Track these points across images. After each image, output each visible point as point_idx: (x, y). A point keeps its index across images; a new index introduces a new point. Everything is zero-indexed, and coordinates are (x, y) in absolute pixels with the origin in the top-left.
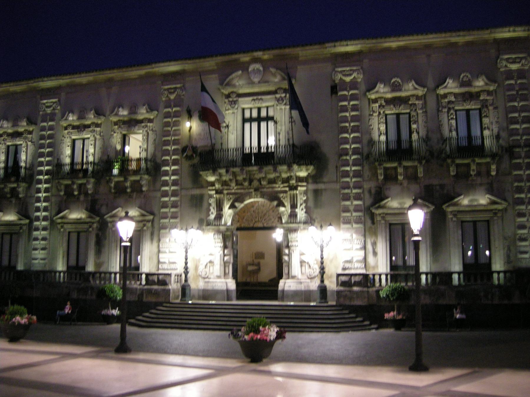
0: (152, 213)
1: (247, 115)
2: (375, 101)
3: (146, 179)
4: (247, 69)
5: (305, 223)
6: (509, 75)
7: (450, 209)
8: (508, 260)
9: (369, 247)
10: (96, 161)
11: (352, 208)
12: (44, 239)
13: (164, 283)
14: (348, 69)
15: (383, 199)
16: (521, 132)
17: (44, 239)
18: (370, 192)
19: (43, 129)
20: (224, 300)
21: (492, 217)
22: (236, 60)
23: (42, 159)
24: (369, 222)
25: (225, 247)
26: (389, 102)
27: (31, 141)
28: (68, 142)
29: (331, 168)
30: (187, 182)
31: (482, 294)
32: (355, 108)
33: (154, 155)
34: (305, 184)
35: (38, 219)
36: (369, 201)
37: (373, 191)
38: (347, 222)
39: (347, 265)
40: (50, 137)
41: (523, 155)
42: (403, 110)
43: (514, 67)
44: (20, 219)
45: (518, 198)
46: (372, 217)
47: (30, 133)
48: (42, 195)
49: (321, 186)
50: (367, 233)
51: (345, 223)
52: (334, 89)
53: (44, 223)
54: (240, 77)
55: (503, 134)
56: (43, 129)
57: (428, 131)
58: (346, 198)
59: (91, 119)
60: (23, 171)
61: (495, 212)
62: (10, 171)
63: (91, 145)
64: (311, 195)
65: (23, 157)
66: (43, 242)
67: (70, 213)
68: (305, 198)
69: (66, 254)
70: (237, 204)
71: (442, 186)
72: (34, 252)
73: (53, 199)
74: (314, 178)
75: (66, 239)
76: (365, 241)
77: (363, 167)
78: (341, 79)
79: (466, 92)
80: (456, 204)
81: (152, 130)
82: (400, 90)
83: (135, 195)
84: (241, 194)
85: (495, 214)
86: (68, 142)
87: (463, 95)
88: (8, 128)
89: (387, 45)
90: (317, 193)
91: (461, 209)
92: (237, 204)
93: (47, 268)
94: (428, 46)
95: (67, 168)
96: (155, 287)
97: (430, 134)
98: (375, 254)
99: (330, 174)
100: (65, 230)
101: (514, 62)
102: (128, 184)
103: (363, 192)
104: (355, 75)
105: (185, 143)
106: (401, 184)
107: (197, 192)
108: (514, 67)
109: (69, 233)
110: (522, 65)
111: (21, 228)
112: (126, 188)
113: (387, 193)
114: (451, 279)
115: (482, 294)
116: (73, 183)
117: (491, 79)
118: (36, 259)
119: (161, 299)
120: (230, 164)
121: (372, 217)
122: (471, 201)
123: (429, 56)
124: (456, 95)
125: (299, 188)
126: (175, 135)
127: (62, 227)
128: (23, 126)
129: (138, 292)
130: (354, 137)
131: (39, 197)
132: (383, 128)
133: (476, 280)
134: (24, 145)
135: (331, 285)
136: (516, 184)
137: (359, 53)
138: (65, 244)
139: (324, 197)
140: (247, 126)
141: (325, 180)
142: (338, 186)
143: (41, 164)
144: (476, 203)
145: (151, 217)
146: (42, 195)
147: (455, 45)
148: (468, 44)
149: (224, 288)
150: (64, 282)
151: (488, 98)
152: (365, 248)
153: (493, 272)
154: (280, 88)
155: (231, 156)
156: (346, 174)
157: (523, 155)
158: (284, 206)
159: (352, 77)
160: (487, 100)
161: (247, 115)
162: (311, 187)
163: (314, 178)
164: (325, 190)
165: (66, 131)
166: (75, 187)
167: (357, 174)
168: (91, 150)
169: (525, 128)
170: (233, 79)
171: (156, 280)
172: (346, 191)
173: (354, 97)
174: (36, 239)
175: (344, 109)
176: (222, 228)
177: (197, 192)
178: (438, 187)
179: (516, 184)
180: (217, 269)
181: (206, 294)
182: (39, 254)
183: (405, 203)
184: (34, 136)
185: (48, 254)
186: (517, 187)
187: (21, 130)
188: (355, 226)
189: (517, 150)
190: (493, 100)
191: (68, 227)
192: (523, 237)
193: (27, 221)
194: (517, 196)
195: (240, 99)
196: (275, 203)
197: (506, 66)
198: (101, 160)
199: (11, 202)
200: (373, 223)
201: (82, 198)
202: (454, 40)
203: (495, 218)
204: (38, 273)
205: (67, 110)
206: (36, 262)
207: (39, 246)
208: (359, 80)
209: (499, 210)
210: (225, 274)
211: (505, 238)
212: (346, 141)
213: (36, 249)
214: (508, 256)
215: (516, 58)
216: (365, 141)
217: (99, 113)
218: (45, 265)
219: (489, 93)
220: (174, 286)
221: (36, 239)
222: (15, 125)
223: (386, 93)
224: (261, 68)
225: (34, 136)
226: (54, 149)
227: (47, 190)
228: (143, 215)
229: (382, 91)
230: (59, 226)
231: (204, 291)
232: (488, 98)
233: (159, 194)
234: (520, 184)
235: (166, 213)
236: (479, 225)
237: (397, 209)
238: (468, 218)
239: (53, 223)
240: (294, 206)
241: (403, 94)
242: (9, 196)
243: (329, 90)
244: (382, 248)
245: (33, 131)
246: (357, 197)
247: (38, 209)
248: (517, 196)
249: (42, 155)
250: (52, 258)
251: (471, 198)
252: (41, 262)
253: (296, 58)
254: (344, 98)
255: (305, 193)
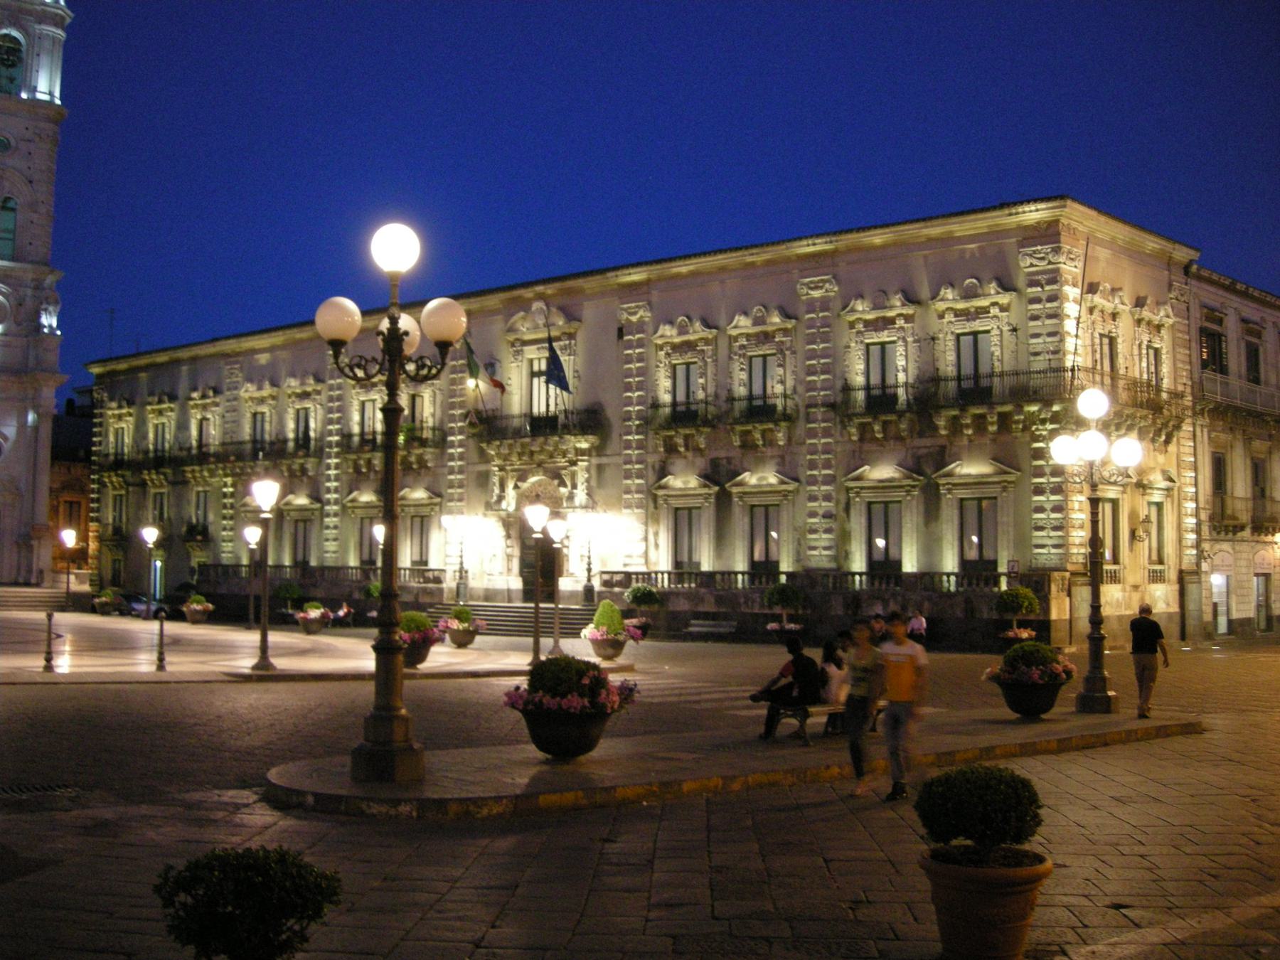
0: (796, 480)
1: (536, 368)
2: (661, 348)
3: (432, 453)
4: (530, 308)
5: (585, 507)
6: (811, 306)
7: (735, 490)
8: (798, 558)
9: (651, 537)
10: (911, 381)
11: (633, 488)
12: (336, 527)
13: (438, 580)
14: (633, 305)
15: (665, 476)
16: (819, 385)
17: (336, 527)
18: (653, 467)
19: (331, 388)
20: (504, 602)
21: (781, 501)
22: (520, 297)
23: (331, 427)
24: (651, 505)
25: (508, 536)
26: (677, 348)
27: (321, 405)
28: (356, 406)
29: (615, 436)
30: (474, 456)
31: (742, 600)
32: (640, 358)
33: (442, 422)
34: (586, 458)
35: (328, 502)
36: (652, 477)
37: (657, 467)
38: (628, 506)
39: (628, 561)
40: (339, 398)
41: (820, 417)
42: (689, 357)
43: (816, 294)
44: (782, 482)
45: (810, 475)
46: (655, 498)
47: (319, 393)
48: (332, 472)
49: (604, 460)
50: (650, 521)
51: (626, 507)
52: (621, 333)
53: (335, 508)
54: (524, 318)
55: (800, 389)
56: (331, 388)
57: (717, 386)
58: (628, 475)
59: (310, 385)
60: (313, 443)
61: (785, 494)
62: (301, 442)
63: (742, 369)
64: (593, 472)
65: (312, 424)
66: (334, 531)
67: (360, 494)
68: (586, 476)
69: (358, 545)
70: (519, 484)
71: (729, 460)
72: (327, 543)
73: (344, 478)
74: (598, 450)
75: (358, 526)
76: (646, 532)
77: (646, 436)
78: (627, 319)
79: (762, 332)
80: (859, 478)
81: (440, 390)
82: (687, 333)
83: (423, 471)
84: (524, 471)
85: (785, 496)
86: (356, 406)
87: (757, 335)
88: (863, 312)
89: (675, 270)
90: (600, 468)
91: (747, 490)
92: (519, 484)
93: (340, 564)
94: (723, 269)
95: (356, 439)
96: (430, 585)
97: (719, 391)
98: (657, 545)
99: (614, 445)
100: (356, 517)
101: (816, 288)
102: (413, 459)
103: (646, 468)
104: (641, 313)
105: (470, 407)
106: (685, 457)
107: (482, 468)
108: (816, 294)
109: (362, 519)
110: (827, 291)
111: (432, 509)
112: (411, 463)
113: (672, 469)
114: (240, 572)
115: (742, 600)
116: (359, 458)
117: (787, 315)
118: (327, 552)
119: (436, 600)
120: (518, 433)
121: (655, 498)
122: (760, 479)
123: (722, 282)
124: (748, 336)
125: (580, 463)
126: (461, 396)
127: (353, 512)
128: (310, 385)
129: (415, 592)
130: (639, 396)
131: (329, 475)
132: (744, 376)
133: (888, 583)
134: (312, 409)
135: (597, 584)
136: (809, 457)
137: (647, 283)
138: (357, 534)
139: (608, 473)
140: (536, 380)
141: (609, 452)
142: (620, 460)
143: (330, 433)
144: (765, 483)
145: (438, 500)
146: (332, 472)
147: (752, 264)
148: (768, 263)
149: (505, 587)
150: (744, 588)
151: (784, 339)
152: (646, 539)
153: (1000, 575)
154: (564, 333)
155: (516, 423)
156: (628, 445)
157: (820, 417)
158: (565, 486)
159: (638, 316)
160: (782, 342)
161: (536, 368)
162: (595, 461)
163: (598, 450)
164: (609, 465)
165: (353, 391)
166: (362, 462)
167: (640, 445)
168: (901, 362)
169: (823, 380)
170: (515, 322)
171: (431, 577)
172: (628, 467)
173: (640, 344)
174: (328, 527)
175: (629, 360)
176: (503, 514)
177: (482, 468)
178: (724, 462)
179: (809, 457)
180: (499, 564)
181: (489, 595)
182: (331, 546)
183: (689, 482)
184: (323, 398)
185: (340, 546)
186: (811, 460)
187: (309, 389)
188: (636, 511)
189: (813, 410)
190: (791, 341)
191: (869, 496)
192: (814, 527)
193: (318, 505)
194: (809, 473)
195: (526, 348)
196: (556, 482)
197: (807, 294)
198: (919, 379)
199: (302, 481)
200: (656, 508)
201: (372, 475)
202: (749, 259)
203: (909, 498)
204: (226, 568)
205: (852, 293)
206: (328, 555)
207: (330, 537)
208: (647, 319)
209: (789, 492)
210: (509, 570)
211: (795, 529)
212: (629, 402)
213: (327, 540)
214: (798, 553)
215: (819, 282)
216: (839, 384)
217: (910, 299)
218: (337, 558)
219: (785, 332)
220: (449, 583)
221: (328, 527)
222: (260, 388)
223: (863, 312)
224: (545, 308)
225: (323, 398)
226: (344, 414)
227: (337, 467)
228: (431, 498)
229: (860, 308)
230: (350, 511)
231: (487, 590)
232: (784, 339)
233: (446, 470)
234: (813, 457)
235: (452, 494)
236: (875, 507)
237: (680, 489)
238: (755, 501)
239: (344, 507)
240: (574, 486)
241: (691, 337)
242: (298, 474)
243: (615, 333)
244: (665, 539)
245: (1009, 305)
246: (640, 475)
247: (328, 491)
248: (809, 473)
249: (331, 422)
250: (343, 550)
251: (760, 475)
252: (334, 555)
253: (580, 291)
254: (630, 345)
255: (588, 470)
